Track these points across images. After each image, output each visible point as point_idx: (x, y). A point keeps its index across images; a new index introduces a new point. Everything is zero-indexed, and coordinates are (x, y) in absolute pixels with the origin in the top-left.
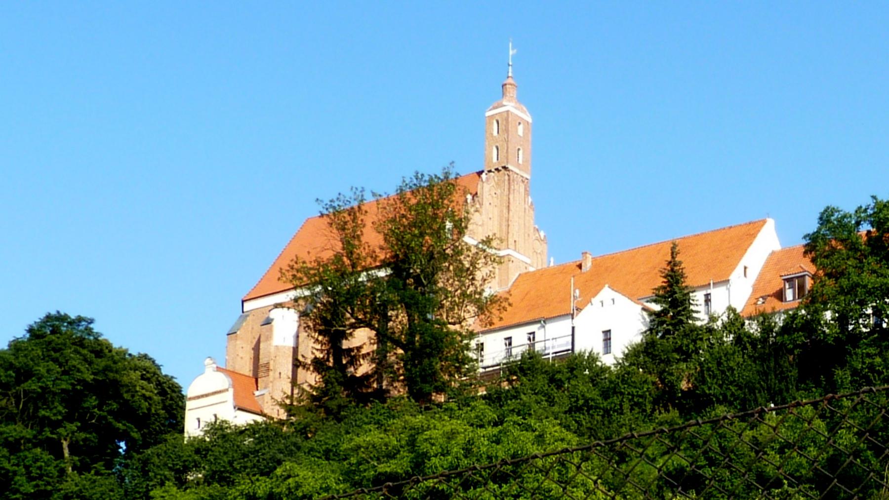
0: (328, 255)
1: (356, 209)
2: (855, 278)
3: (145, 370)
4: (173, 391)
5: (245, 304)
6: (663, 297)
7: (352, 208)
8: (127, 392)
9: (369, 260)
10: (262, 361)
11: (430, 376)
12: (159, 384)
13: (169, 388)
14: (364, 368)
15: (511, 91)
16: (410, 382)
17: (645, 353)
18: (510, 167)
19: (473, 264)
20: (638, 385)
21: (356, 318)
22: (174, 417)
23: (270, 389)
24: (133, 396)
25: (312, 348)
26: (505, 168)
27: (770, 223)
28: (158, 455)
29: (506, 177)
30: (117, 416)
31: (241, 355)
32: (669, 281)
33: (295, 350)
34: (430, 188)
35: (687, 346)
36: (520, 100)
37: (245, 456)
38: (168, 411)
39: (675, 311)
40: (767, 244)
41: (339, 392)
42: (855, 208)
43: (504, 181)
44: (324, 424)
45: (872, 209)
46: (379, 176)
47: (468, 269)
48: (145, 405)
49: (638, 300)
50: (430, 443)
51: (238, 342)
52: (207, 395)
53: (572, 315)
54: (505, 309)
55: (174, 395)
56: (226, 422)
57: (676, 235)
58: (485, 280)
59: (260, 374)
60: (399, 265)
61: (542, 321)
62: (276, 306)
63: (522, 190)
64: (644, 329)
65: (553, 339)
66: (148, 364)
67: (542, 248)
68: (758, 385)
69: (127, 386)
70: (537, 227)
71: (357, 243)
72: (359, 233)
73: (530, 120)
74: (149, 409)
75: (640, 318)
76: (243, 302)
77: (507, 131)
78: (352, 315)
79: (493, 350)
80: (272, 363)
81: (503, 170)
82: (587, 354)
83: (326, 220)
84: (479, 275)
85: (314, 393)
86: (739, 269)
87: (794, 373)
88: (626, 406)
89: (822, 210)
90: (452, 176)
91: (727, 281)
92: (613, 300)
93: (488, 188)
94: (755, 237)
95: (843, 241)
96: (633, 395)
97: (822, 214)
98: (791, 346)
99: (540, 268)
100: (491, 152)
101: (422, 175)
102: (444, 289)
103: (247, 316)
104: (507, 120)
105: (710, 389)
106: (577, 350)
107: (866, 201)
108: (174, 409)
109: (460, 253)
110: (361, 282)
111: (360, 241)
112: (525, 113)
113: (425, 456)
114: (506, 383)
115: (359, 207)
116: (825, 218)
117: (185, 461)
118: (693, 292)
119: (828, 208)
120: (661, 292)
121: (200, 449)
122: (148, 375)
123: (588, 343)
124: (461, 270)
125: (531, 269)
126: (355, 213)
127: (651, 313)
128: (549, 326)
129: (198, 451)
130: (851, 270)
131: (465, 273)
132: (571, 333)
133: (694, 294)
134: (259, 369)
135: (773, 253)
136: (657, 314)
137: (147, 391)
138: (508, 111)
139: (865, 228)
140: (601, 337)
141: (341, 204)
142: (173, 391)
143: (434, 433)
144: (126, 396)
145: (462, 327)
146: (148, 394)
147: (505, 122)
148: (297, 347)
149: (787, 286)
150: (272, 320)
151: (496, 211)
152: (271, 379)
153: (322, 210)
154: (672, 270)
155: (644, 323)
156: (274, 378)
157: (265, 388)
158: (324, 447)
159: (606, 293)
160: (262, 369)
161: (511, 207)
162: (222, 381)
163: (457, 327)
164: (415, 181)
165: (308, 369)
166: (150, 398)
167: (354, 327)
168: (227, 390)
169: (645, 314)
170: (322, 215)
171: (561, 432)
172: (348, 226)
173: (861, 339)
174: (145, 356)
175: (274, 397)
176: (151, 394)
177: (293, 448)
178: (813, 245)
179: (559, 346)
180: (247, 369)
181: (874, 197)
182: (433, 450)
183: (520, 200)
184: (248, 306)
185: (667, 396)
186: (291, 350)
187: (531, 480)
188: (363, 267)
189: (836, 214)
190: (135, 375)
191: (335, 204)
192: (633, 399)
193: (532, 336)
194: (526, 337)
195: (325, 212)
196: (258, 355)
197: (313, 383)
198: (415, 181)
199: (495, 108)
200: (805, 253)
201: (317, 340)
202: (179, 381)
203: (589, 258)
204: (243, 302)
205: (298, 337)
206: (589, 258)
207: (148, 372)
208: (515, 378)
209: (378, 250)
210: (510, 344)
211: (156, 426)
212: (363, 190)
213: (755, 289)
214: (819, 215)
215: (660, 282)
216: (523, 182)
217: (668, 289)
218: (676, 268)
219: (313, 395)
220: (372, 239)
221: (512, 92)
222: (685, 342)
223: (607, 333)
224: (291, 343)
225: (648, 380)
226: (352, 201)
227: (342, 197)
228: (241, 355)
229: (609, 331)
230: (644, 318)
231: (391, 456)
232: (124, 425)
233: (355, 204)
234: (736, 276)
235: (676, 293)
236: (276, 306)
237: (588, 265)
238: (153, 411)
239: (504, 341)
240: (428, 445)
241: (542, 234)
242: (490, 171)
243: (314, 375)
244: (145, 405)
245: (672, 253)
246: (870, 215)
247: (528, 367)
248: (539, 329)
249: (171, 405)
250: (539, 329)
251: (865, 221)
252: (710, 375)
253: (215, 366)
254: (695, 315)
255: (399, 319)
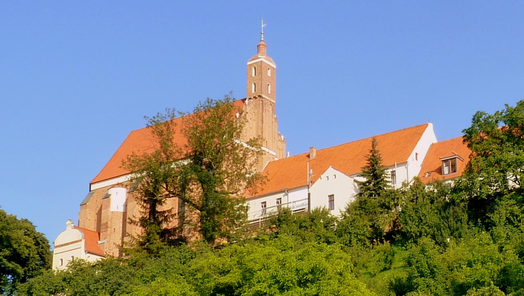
0: (150, 152)
1: (170, 122)
2: (499, 157)
3: (27, 229)
4: (44, 243)
5: (92, 186)
6: (367, 172)
7: (167, 122)
8: (15, 243)
9: (177, 154)
10: (103, 221)
11: (216, 227)
12: (35, 238)
13: (41, 240)
14: (174, 223)
15: (263, 49)
16: (204, 231)
17: (360, 206)
18: (263, 96)
19: (244, 155)
20: (361, 228)
21: (169, 192)
22: (43, 259)
23: (108, 239)
24: (19, 246)
25: (138, 211)
26: (259, 96)
27: (430, 126)
28: (39, 283)
29: (261, 102)
30: (9, 259)
31: (89, 218)
32: (371, 163)
33: (125, 214)
34: (218, 107)
35: (389, 203)
36: (269, 55)
37: (97, 281)
38: (40, 256)
39: (376, 181)
40: (429, 138)
41: (158, 237)
42: (495, 112)
43: (259, 105)
44: (147, 260)
45: (506, 112)
46: (185, 99)
47: (242, 158)
48: (27, 251)
49: (350, 176)
50: (254, 262)
51: (87, 210)
52: (67, 244)
53: (308, 186)
54: (265, 183)
55: (44, 245)
56: (83, 260)
57: (377, 133)
58: (252, 165)
59: (102, 230)
60: (197, 158)
61: (286, 191)
62: (113, 186)
63: (271, 110)
64: (356, 194)
65: (295, 201)
66: (29, 225)
67: (283, 146)
68: (442, 225)
69: (16, 239)
70: (279, 132)
71: (170, 143)
72: (171, 137)
73: (275, 67)
74: (29, 254)
75: (353, 186)
76: (90, 184)
77: (261, 73)
78: (167, 189)
79: (255, 211)
80: (109, 222)
81: (259, 98)
82: (321, 210)
83: (151, 129)
84: (248, 162)
85: (141, 240)
86: (413, 155)
87: (465, 217)
88: (354, 241)
89: (474, 114)
90: (231, 101)
91: (406, 163)
92: (335, 175)
93: (249, 108)
94: (421, 135)
95: (488, 133)
96: (357, 234)
97: (475, 116)
98: (458, 201)
99: (281, 158)
100: (251, 87)
101: (212, 100)
102: (226, 172)
103: (93, 193)
104: (261, 67)
105: (411, 228)
106: (313, 208)
107: (501, 108)
108: (43, 254)
109: (235, 149)
110: (172, 168)
111: (172, 142)
112: (271, 62)
113: (251, 272)
114: (268, 230)
115: (171, 121)
116: (476, 119)
117: (56, 286)
118: (387, 169)
119: (478, 112)
120: (366, 170)
121: (66, 279)
122: (29, 232)
123: (319, 202)
124: (237, 159)
125: (276, 159)
126: (169, 125)
127: (360, 183)
128: (290, 194)
129: (64, 280)
130: (495, 151)
131: (240, 161)
132: (307, 197)
133: (387, 171)
134: (100, 227)
135: (433, 145)
136: (364, 184)
137: (28, 242)
138: (261, 61)
139: (501, 125)
140: (328, 199)
141: (159, 119)
142: (44, 243)
143: (257, 255)
144: (15, 246)
145: (238, 195)
146: (28, 244)
147: (260, 68)
148: (126, 212)
149: (444, 166)
150: (110, 195)
151: (254, 122)
152: (109, 233)
153: (148, 123)
154: (373, 155)
155: (355, 190)
156: (111, 232)
157: (105, 239)
158: (151, 274)
159: (330, 171)
160: (102, 227)
161: (264, 120)
162: (78, 235)
163: (235, 195)
164: (207, 104)
165: (137, 225)
166: (30, 247)
167: (167, 196)
168: (81, 240)
169: (356, 184)
170: (148, 126)
171: (340, 253)
172: (164, 133)
173: (504, 195)
174: (26, 220)
175: (111, 245)
176: (30, 245)
177: (129, 275)
178: (469, 136)
179: (297, 207)
180: (92, 226)
181: (506, 105)
182: (257, 267)
183: (269, 116)
184: (93, 187)
185: (377, 235)
186: (122, 214)
187: (325, 284)
188: (174, 159)
189: (484, 116)
190: (21, 233)
191: (156, 120)
192: (357, 236)
193: (279, 201)
194: (276, 201)
195: (150, 124)
196: (101, 218)
197: (140, 234)
198: (207, 104)
199: (254, 59)
200: (464, 141)
201: (143, 206)
202: (47, 237)
203: (315, 150)
204: (90, 184)
205: (126, 206)
206: (315, 150)
207: (28, 230)
208: (274, 226)
209: (183, 148)
210: (265, 206)
211: (33, 265)
212: (174, 110)
213: (423, 166)
214: (472, 117)
215: (365, 163)
216: (271, 105)
217: (371, 168)
218: (375, 155)
219: (140, 242)
220: (180, 141)
221: (263, 50)
222: (387, 200)
223: (331, 197)
224: (121, 209)
225: (364, 225)
226: (167, 117)
227: (160, 115)
228: (89, 218)
229: (333, 195)
230: (355, 187)
231: (224, 273)
232: (13, 264)
233: (169, 119)
234: (411, 159)
235: (376, 170)
236: (113, 186)
237: (314, 155)
238: (31, 256)
239: (261, 205)
240: (253, 263)
241: (282, 137)
242: (250, 99)
243: (141, 228)
244: (27, 251)
245: (373, 145)
246: (504, 117)
247: (281, 220)
248: (284, 196)
249: (42, 252)
250: (284, 196)
251: (501, 120)
252: (410, 219)
253: (73, 225)
254: (388, 184)
255: (195, 191)
